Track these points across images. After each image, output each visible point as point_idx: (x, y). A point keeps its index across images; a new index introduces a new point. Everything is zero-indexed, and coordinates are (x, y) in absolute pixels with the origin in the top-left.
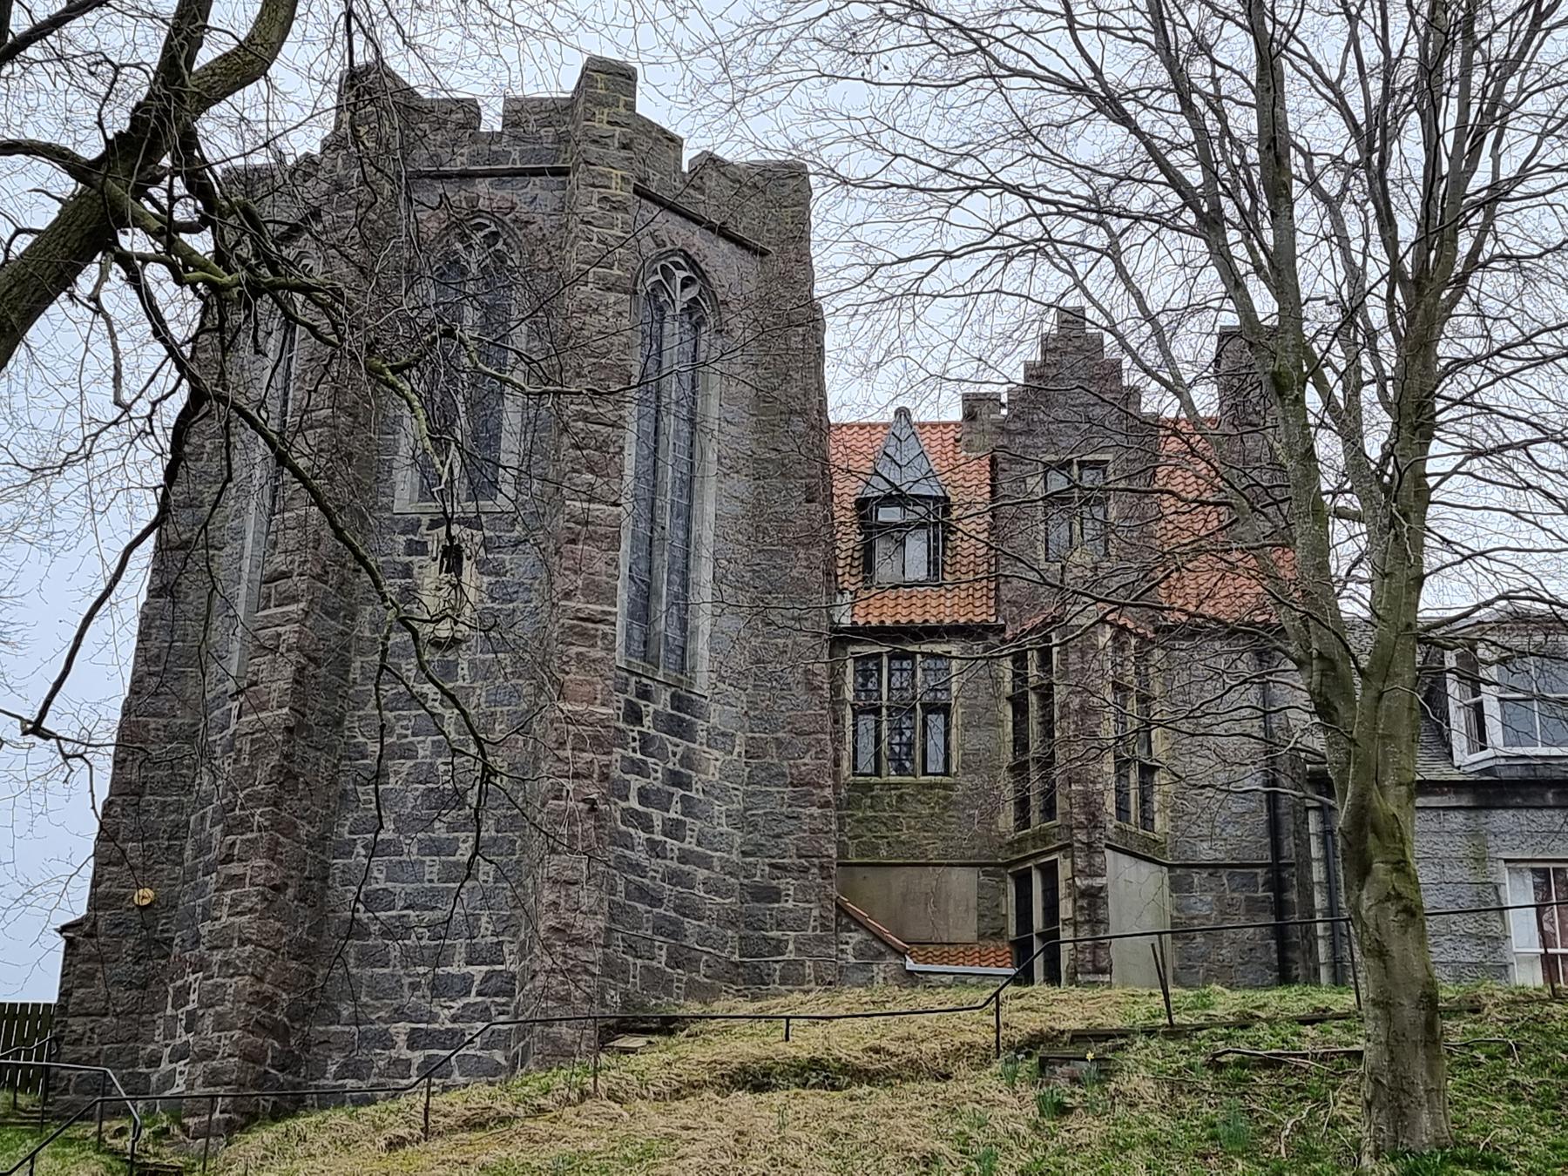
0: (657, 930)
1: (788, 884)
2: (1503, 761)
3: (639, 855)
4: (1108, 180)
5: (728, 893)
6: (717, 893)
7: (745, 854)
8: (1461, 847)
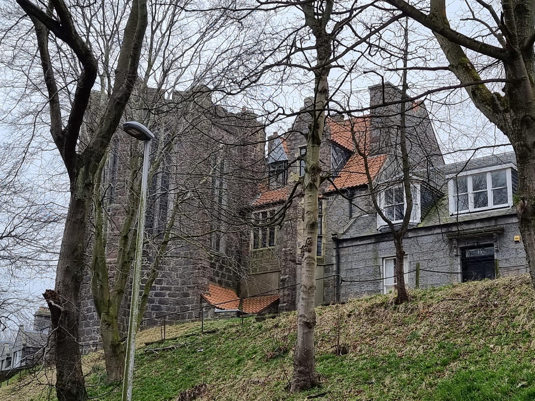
0: (152, 309)
1: (190, 292)
6: (173, 297)
7: (182, 285)
8: (371, 255)
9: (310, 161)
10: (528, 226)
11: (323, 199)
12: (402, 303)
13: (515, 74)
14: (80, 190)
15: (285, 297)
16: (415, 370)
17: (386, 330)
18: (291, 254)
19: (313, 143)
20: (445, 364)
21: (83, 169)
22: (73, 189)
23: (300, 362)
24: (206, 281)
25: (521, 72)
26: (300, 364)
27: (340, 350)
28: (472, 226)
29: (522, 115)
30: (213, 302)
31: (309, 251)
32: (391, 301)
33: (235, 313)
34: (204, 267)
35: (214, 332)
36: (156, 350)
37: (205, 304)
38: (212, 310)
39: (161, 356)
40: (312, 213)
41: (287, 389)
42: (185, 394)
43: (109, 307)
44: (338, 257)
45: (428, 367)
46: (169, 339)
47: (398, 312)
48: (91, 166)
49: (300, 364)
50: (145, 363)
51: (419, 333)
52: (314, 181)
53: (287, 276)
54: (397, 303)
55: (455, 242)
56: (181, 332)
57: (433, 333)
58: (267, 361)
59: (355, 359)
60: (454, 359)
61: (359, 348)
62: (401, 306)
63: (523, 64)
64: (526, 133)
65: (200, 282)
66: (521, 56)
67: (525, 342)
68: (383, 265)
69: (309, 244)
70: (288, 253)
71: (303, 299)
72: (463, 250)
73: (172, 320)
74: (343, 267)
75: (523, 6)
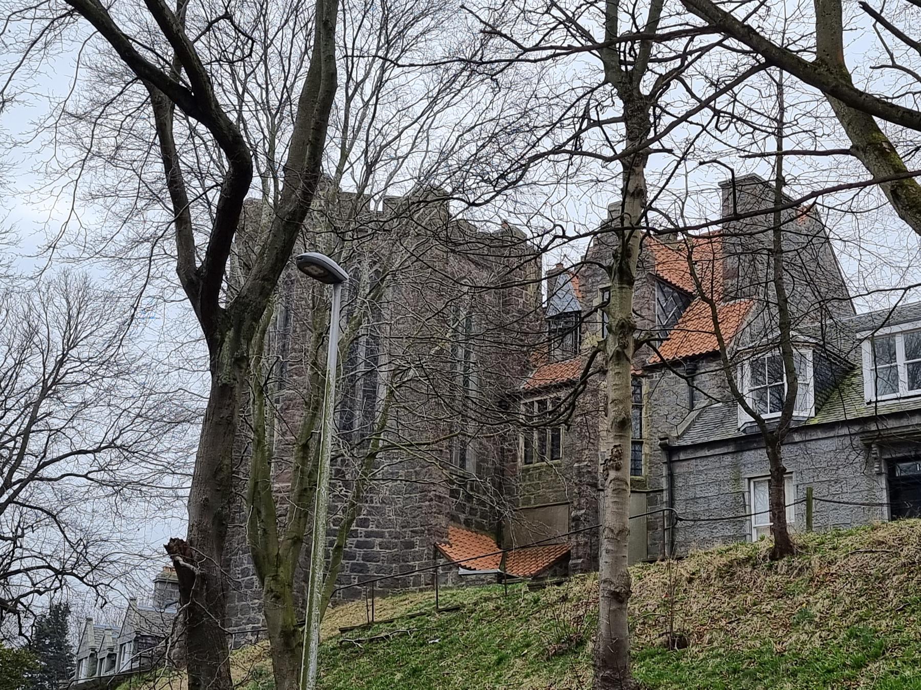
0: (352, 570)
1: (417, 539)
2: (749, 425)
4: (455, 196)
5: (395, 546)
6: (387, 548)
7: (403, 527)
9: (617, 313)
11: (643, 376)
12: (782, 557)
15: (580, 548)
17: (755, 605)
18: (589, 472)
19: (621, 281)
21: (230, 334)
22: (215, 368)
24: (443, 520)
26: (605, 665)
27: (674, 641)
28: (904, 422)
30: (455, 558)
31: (618, 468)
32: (763, 553)
33: (493, 576)
34: (440, 497)
35: (457, 609)
36: (359, 642)
37: (442, 561)
38: (454, 570)
39: (367, 651)
40: (621, 402)
43: (278, 567)
44: (671, 477)
45: (829, 671)
46: (381, 622)
47: (776, 573)
48: (245, 328)
49: (605, 665)
50: (341, 664)
51: (813, 611)
52: (624, 346)
53: (583, 511)
55: (875, 449)
56: (401, 610)
57: (838, 610)
59: (701, 656)
60: (876, 657)
61: (707, 637)
62: (782, 564)
68: (749, 492)
69: (616, 457)
70: (585, 470)
72: (891, 465)
73: (387, 590)
74: (680, 496)
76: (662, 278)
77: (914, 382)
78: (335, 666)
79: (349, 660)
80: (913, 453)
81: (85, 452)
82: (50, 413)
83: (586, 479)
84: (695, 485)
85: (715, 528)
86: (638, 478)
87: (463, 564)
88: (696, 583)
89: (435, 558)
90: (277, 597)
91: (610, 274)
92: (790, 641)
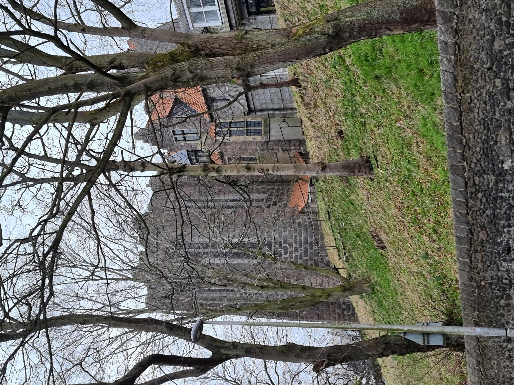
0: (312, 248)
1: (297, 221)
3: (298, 254)
5: (300, 231)
10: (253, 73)
12: (299, 83)
13: (141, 91)
14: (238, 352)
16: (354, 90)
17: (322, 99)
20: (347, 69)
21: (223, 351)
22: (237, 357)
23: (351, 172)
24: (287, 210)
25: (140, 87)
28: (230, 8)
29: (171, 83)
30: (303, 204)
31: (268, 170)
34: (277, 212)
35: (328, 212)
36: (345, 254)
37: (306, 210)
38: (309, 204)
40: (238, 169)
41: (372, 180)
42: (378, 246)
43: (316, 296)
44: (262, 110)
45: (351, 81)
48: (219, 345)
51: (324, 79)
52: (214, 169)
53: (280, 148)
54: (300, 86)
55: (244, 22)
56: (330, 232)
57: (323, 68)
58: (350, 185)
59: (346, 127)
60: (343, 61)
61: (338, 122)
62: (303, 84)
63: (133, 85)
64: (184, 78)
65: (288, 214)
66: (128, 87)
67: (328, 10)
68: (267, 76)
70: (261, 148)
71: (304, 173)
72: (250, 14)
74: (270, 106)
75: (88, 84)
76: (169, 114)
77: (211, 3)
78: (356, 266)
79: (353, 260)
80: (245, 5)
81: (265, 365)
82: (249, 381)
83: (265, 147)
84: (265, 100)
85: (284, 90)
86: (263, 122)
87: (306, 201)
88: (313, 119)
89: (305, 213)
90: (329, 295)
91: (181, 176)
92: (339, 91)
